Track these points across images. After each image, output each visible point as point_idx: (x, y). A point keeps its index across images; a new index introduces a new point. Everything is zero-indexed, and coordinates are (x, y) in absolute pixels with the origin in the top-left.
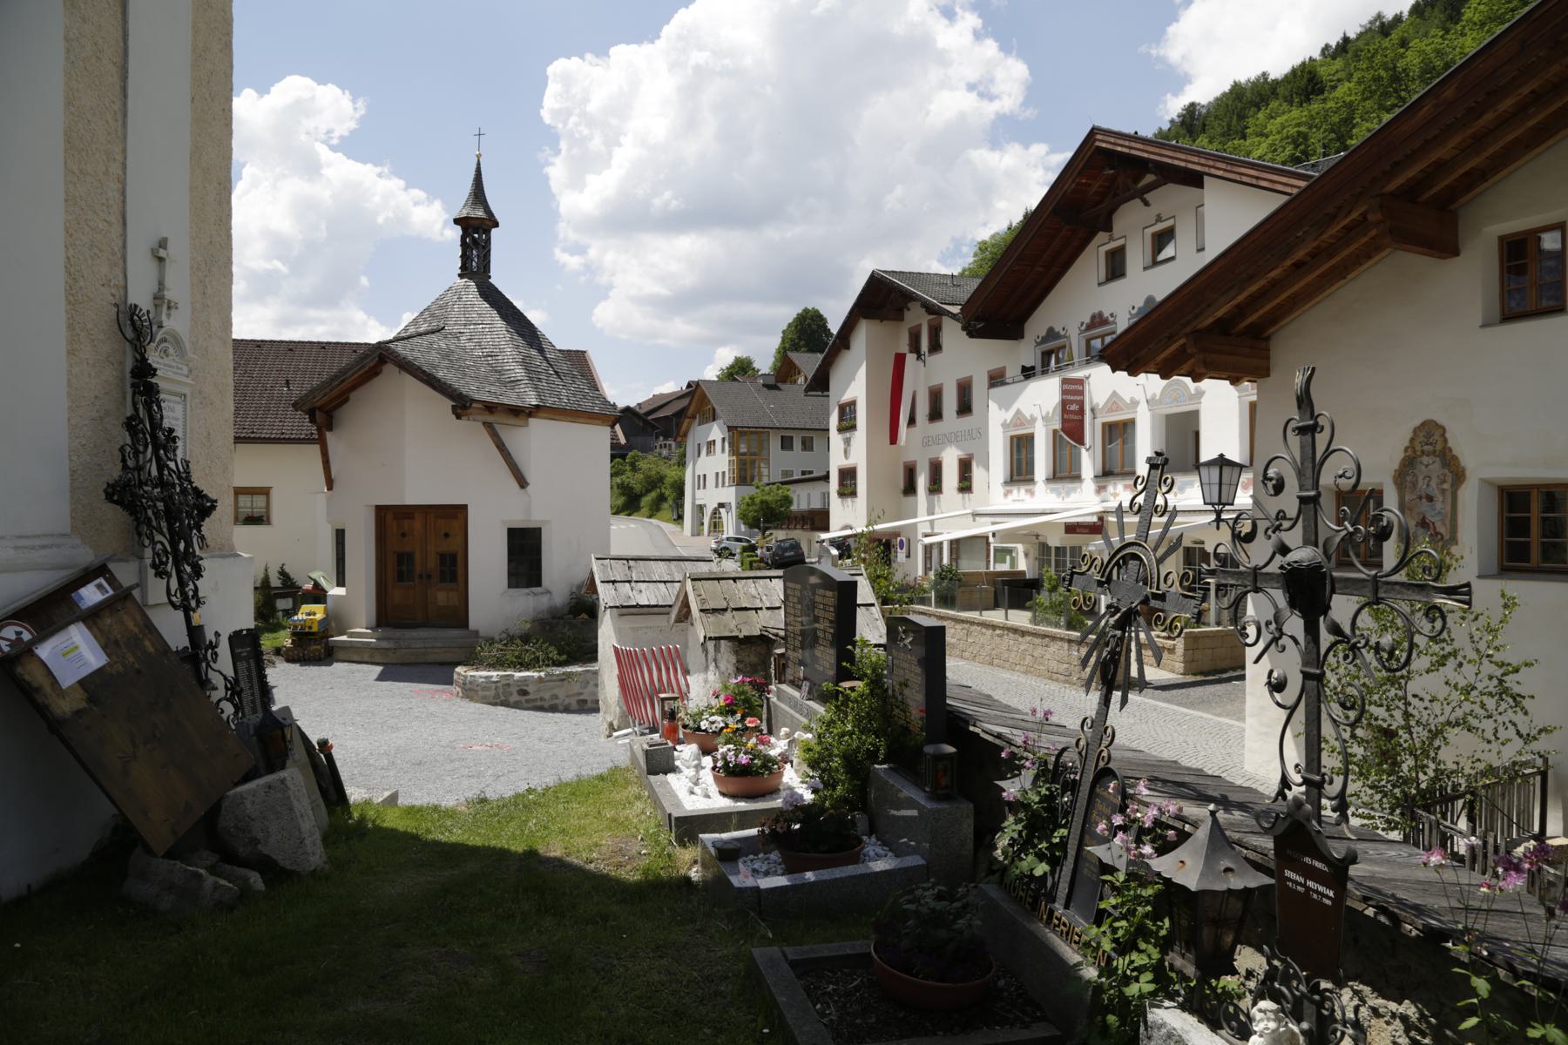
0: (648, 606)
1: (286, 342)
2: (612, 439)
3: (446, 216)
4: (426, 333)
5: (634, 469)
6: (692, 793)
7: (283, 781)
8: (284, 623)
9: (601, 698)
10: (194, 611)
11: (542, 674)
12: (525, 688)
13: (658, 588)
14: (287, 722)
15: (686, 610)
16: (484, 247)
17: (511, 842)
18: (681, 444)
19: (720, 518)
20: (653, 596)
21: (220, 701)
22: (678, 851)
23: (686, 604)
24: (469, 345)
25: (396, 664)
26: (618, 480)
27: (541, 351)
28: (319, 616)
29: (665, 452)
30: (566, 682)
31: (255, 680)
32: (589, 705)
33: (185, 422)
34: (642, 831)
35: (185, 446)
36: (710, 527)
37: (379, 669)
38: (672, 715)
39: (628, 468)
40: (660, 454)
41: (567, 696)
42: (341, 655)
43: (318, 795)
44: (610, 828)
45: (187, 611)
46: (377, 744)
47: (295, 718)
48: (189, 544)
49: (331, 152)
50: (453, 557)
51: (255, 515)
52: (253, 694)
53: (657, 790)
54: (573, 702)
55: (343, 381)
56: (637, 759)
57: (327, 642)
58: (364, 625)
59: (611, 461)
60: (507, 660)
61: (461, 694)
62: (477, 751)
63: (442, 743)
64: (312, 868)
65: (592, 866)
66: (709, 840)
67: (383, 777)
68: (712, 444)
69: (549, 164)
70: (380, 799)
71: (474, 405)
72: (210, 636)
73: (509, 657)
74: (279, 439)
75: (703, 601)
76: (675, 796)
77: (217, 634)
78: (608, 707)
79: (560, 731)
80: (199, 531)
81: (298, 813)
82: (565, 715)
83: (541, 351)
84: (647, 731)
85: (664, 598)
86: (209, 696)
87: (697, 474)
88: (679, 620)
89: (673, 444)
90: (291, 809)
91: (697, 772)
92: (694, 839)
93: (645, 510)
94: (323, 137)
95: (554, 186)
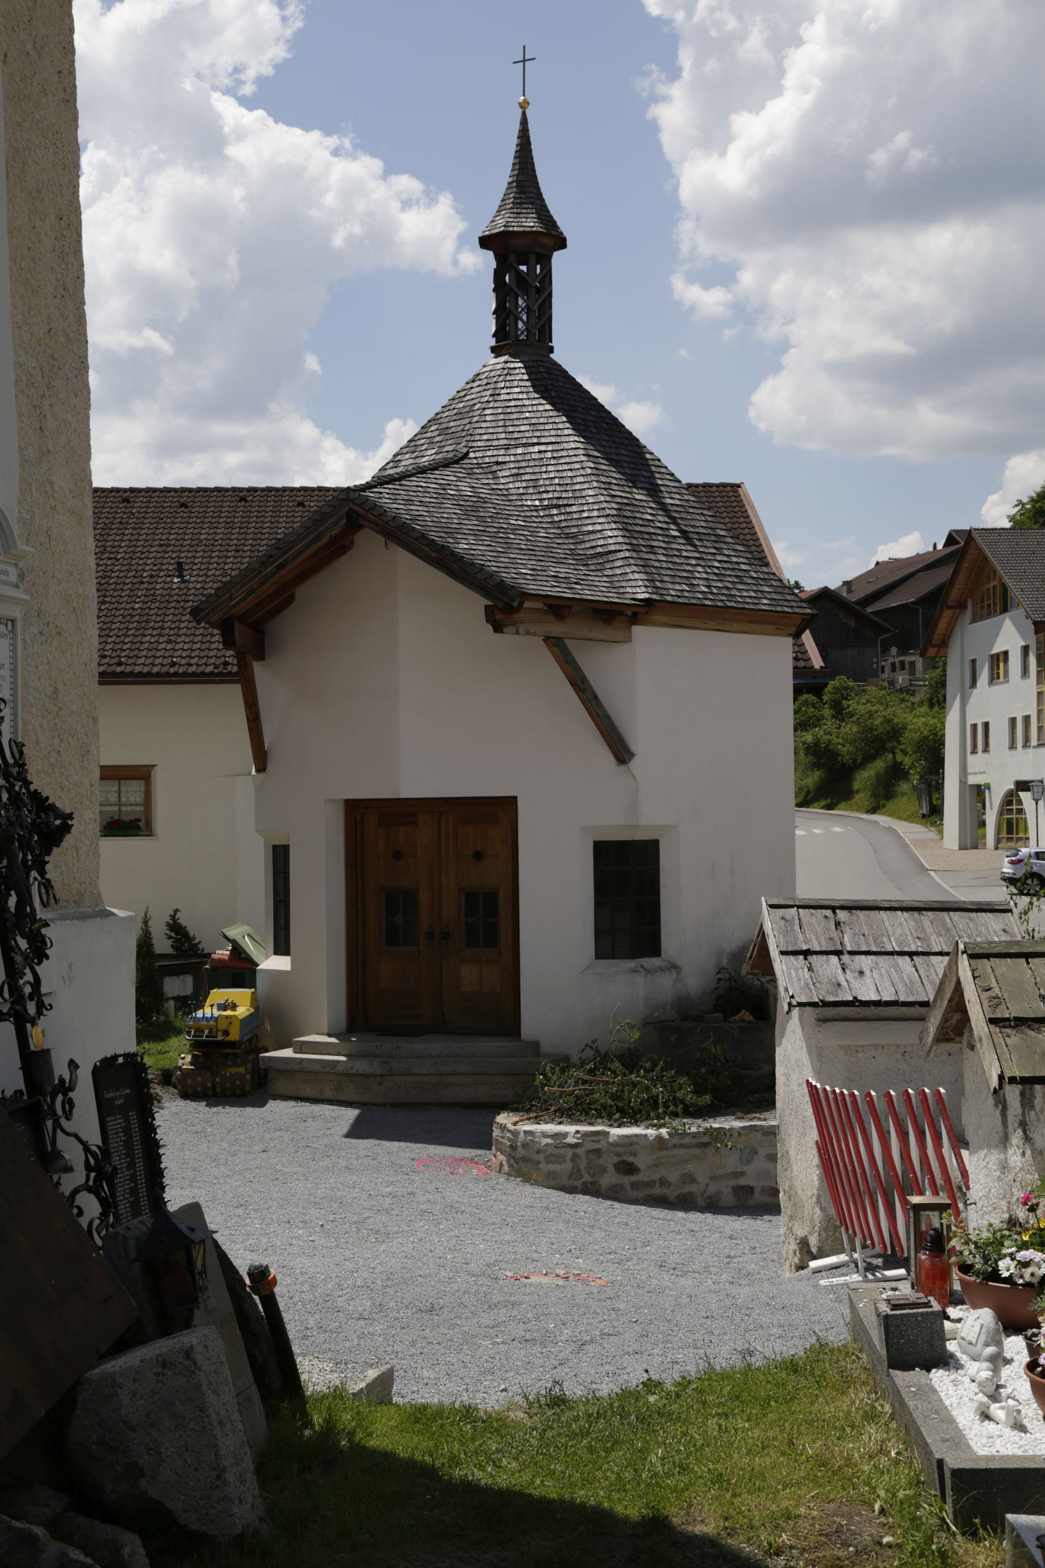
0: (878, 1003)
1: (175, 490)
2: (796, 659)
3: (462, 226)
4: (434, 467)
5: (840, 713)
6: (986, 1416)
7: (188, 1353)
8: (178, 1024)
9: (783, 1186)
10: (33, 1022)
11: (664, 1132)
12: (631, 1159)
13: (896, 966)
14: (196, 1237)
15: (957, 1017)
16: (538, 291)
17: (615, 1496)
18: (937, 663)
19: (1020, 811)
20: (887, 984)
21: (76, 1191)
22: (962, 1545)
23: (958, 1005)
25: (384, 1105)
26: (808, 737)
27: (654, 491)
28: (243, 1011)
29: (901, 679)
30: (710, 1150)
31: (138, 1152)
32: (758, 1197)
34: (882, 1493)
35: (15, 715)
36: (998, 831)
37: (352, 1113)
39: (827, 712)
40: (892, 683)
41: (714, 1178)
42: (281, 1085)
43: (248, 1378)
45: (21, 1022)
47: (212, 1227)
48: (25, 898)
49: (243, 111)
50: (491, 898)
51: (126, 818)
52: (133, 1178)
53: (911, 1404)
54: (725, 1189)
55: (281, 567)
56: (866, 1331)
58: (326, 1031)
59: (795, 700)
61: (506, 1168)
62: (540, 1286)
63: (473, 1267)
66: (1028, 1528)
67: (362, 1336)
68: (1000, 659)
69: (656, 99)
70: (363, 1385)
72: (60, 1069)
73: (599, 1096)
74: (167, 674)
75: (996, 1001)
77: (73, 1065)
78: (797, 1205)
79: (700, 1249)
80: (42, 872)
83: (654, 491)
84: (879, 1261)
85: (910, 988)
86: (58, 1184)
87: (970, 722)
88: (944, 1036)
89: (919, 663)
91: (996, 1371)
92: (997, 1526)
93: (861, 798)
94: (227, 81)
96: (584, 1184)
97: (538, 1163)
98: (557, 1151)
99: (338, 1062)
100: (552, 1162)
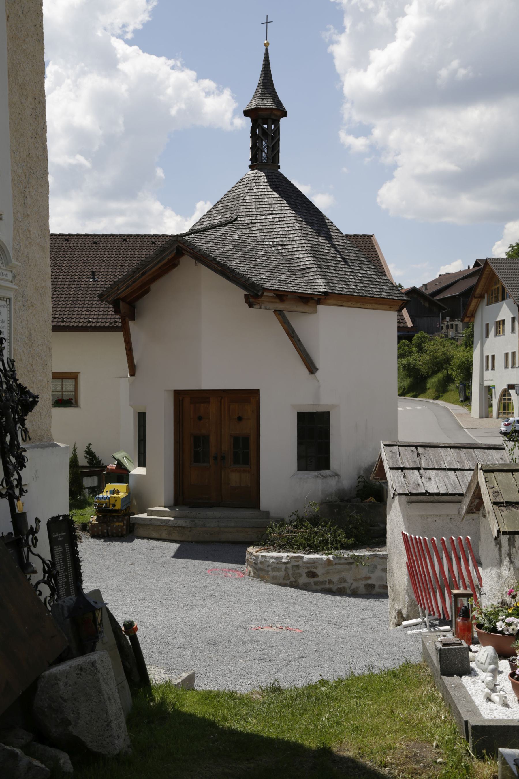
0: (438, 494)
1: (91, 235)
2: (399, 322)
4: (220, 225)
5: (420, 349)
6: (489, 700)
7: (93, 664)
8: (90, 500)
9: (390, 584)
10: (18, 499)
11: (331, 557)
12: (314, 570)
13: (447, 476)
14: (98, 606)
15: (477, 501)
16: (273, 138)
17: (305, 737)
18: (469, 325)
19: (510, 399)
20: (443, 484)
21: (38, 583)
22: (476, 763)
23: (478, 496)
24: (261, 235)
25: (192, 542)
26: (405, 361)
27: (329, 238)
28: (122, 494)
29: (451, 333)
30: (353, 566)
31: (69, 564)
32: (377, 590)
33: (10, 324)
34: (437, 737)
35: (10, 346)
36: (499, 409)
37: (176, 546)
38: (466, 613)
39: (414, 349)
40: (446, 335)
41: (355, 580)
42: (141, 531)
44: (404, 731)
45: (12, 499)
46: (174, 621)
48: (14, 437)
49: (127, 46)
50: (246, 439)
51: (65, 398)
52: (67, 577)
53: (452, 693)
54: (361, 586)
55: (143, 274)
56: (430, 657)
57: (129, 519)
58: (163, 505)
59: (398, 343)
60: (297, 541)
61: (252, 574)
62: (268, 632)
63: (235, 623)
64: (117, 752)
65: (386, 771)
66: (510, 755)
69: (333, 42)
71: (266, 294)
72: (31, 523)
74: (86, 327)
75: (497, 494)
76: (472, 702)
77: (37, 520)
78: (397, 594)
80: (23, 425)
81: (106, 696)
82: (353, 599)
83: (329, 238)
84: (437, 622)
85: (454, 486)
86: (30, 579)
87: (485, 355)
88: (470, 511)
90: (100, 691)
91: (494, 677)
92: (494, 754)
94: (119, 32)
95: (338, 64)
96: (291, 582)
97: (268, 571)
98: (277, 566)
99: (169, 520)
100: (275, 571)
